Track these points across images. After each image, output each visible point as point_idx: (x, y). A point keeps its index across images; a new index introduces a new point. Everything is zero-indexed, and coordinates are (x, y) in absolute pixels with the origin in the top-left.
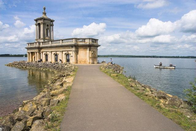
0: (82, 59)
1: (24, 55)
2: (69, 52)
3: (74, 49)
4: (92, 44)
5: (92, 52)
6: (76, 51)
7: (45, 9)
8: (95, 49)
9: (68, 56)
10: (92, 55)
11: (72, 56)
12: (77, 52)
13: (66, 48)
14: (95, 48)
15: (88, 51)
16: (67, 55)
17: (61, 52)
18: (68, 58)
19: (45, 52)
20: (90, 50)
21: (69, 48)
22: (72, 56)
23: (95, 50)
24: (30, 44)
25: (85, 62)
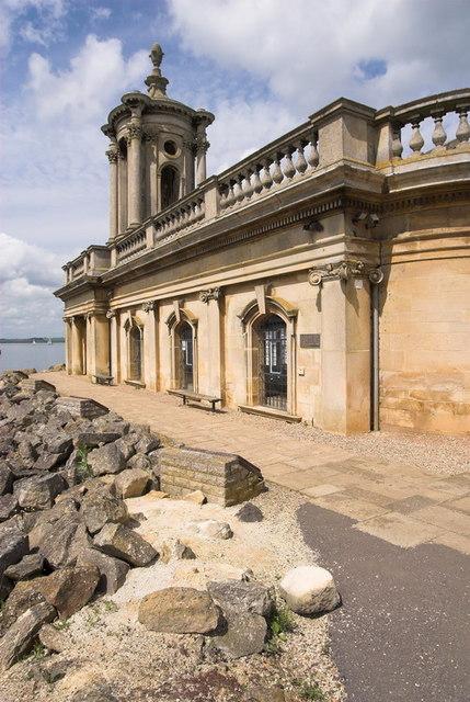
2: (286, 294)
3: (332, 248)
6: (363, 275)
9: (269, 336)
11: (312, 341)
13: (255, 248)
16: (268, 324)
17: (214, 303)
18: (271, 361)
19: (169, 301)
21: (284, 248)
22: (312, 341)
24: (114, 252)
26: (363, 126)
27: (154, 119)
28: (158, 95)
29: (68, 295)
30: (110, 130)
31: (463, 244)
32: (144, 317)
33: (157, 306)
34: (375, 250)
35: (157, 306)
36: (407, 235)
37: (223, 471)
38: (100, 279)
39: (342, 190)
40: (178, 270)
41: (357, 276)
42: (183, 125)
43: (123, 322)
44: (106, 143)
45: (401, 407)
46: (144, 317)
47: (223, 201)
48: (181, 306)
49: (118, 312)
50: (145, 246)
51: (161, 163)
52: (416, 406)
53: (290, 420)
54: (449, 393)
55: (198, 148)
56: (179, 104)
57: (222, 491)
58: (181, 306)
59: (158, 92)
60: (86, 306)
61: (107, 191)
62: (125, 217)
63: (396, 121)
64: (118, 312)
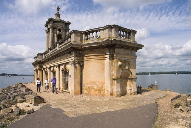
0: (93, 83)
1: (149, 73)
3: (72, 58)
4: (115, 40)
5: (120, 63)
6: (78, 63)
7: (58, 9)
8: (128, 54)
10: (117, 72)
12: (80, 64)
14: (129, 51)
15: (107, 61)
19: (62, 65)
20: (112, 58)
23: (127, 58)
25: (100, 90)
26: (79, 34)
27: (56, 24)
28: (58, 18)
29: (34, 64)
30: (46, 26)
31: (95, 57)
32: (56, 69)
33: (59, 66)
34: (82, 58)
35: (59, 66)
36: (87, 55)
37: (34, 98)
38: (40, 61)
39: (72, 47)
40: (53, 60)
41: (77, 63)
42: (63, 25)
43: (61, 69)
44: (46, 28)
45: (86, 89)
46: (56, 69)
47: (60, 46)
48: (65, 66)
49: (44, 69)
50: (57, 49)
51: (57, 34)
52: (88, 89)
53: (68, 92)
54: (93, 87)
55: (66, 30)
56: (63, 21)
57: (33, 101)
58: (65, 66)
59: (58, 17)
60: (37, 68)
61: (46, 39)
62: (49, 45)
63: (87, 33)
64: (44, 69)
